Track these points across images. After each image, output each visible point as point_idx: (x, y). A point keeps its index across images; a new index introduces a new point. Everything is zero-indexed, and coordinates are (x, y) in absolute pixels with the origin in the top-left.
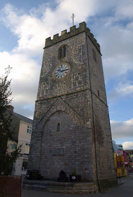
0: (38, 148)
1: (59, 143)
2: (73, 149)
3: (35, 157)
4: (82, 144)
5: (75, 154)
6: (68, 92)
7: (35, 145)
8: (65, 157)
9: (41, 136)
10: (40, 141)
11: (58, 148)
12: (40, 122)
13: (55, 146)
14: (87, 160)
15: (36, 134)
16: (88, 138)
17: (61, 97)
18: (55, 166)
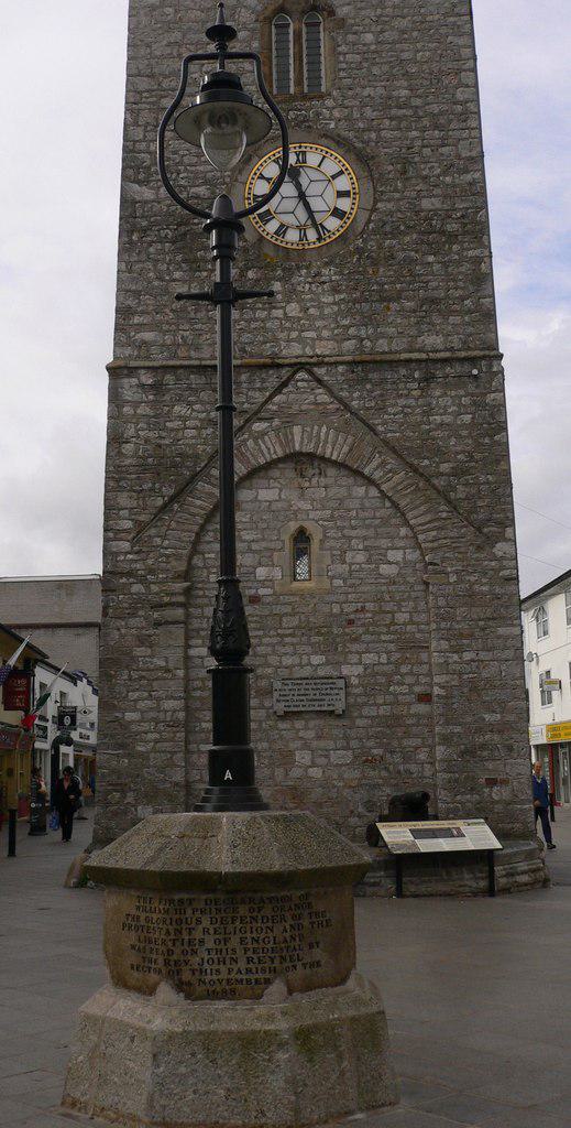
0: (168, 671)
1: (312, 645)
2: (409, 679)
3: (145, 726)
4: (467, 656)
5: (422, 708)
6: (360, 349)
7: (139, 651)
8: (359, 722)
9: (181, 599)
10: (179, 631)
11: (307, 672)
12: (164, 508)
13: (287, 661)
14: (496, 737)
15: (136, 588)
16: (501, 631)
17: (311, 373)
18: (296, 772)
